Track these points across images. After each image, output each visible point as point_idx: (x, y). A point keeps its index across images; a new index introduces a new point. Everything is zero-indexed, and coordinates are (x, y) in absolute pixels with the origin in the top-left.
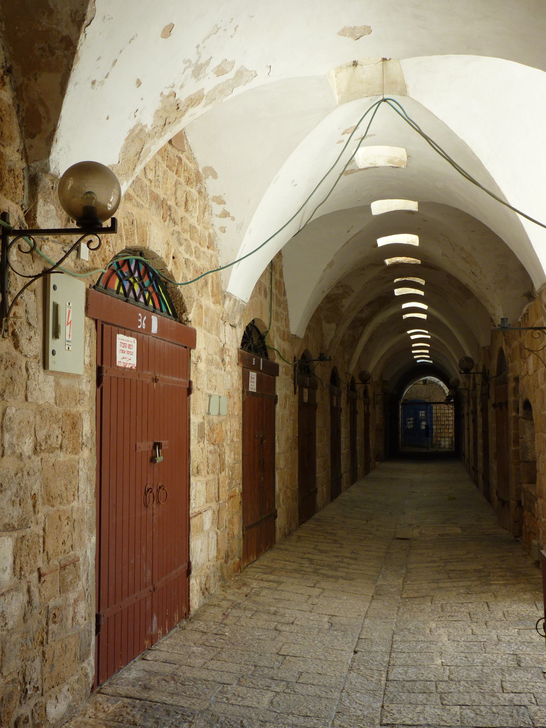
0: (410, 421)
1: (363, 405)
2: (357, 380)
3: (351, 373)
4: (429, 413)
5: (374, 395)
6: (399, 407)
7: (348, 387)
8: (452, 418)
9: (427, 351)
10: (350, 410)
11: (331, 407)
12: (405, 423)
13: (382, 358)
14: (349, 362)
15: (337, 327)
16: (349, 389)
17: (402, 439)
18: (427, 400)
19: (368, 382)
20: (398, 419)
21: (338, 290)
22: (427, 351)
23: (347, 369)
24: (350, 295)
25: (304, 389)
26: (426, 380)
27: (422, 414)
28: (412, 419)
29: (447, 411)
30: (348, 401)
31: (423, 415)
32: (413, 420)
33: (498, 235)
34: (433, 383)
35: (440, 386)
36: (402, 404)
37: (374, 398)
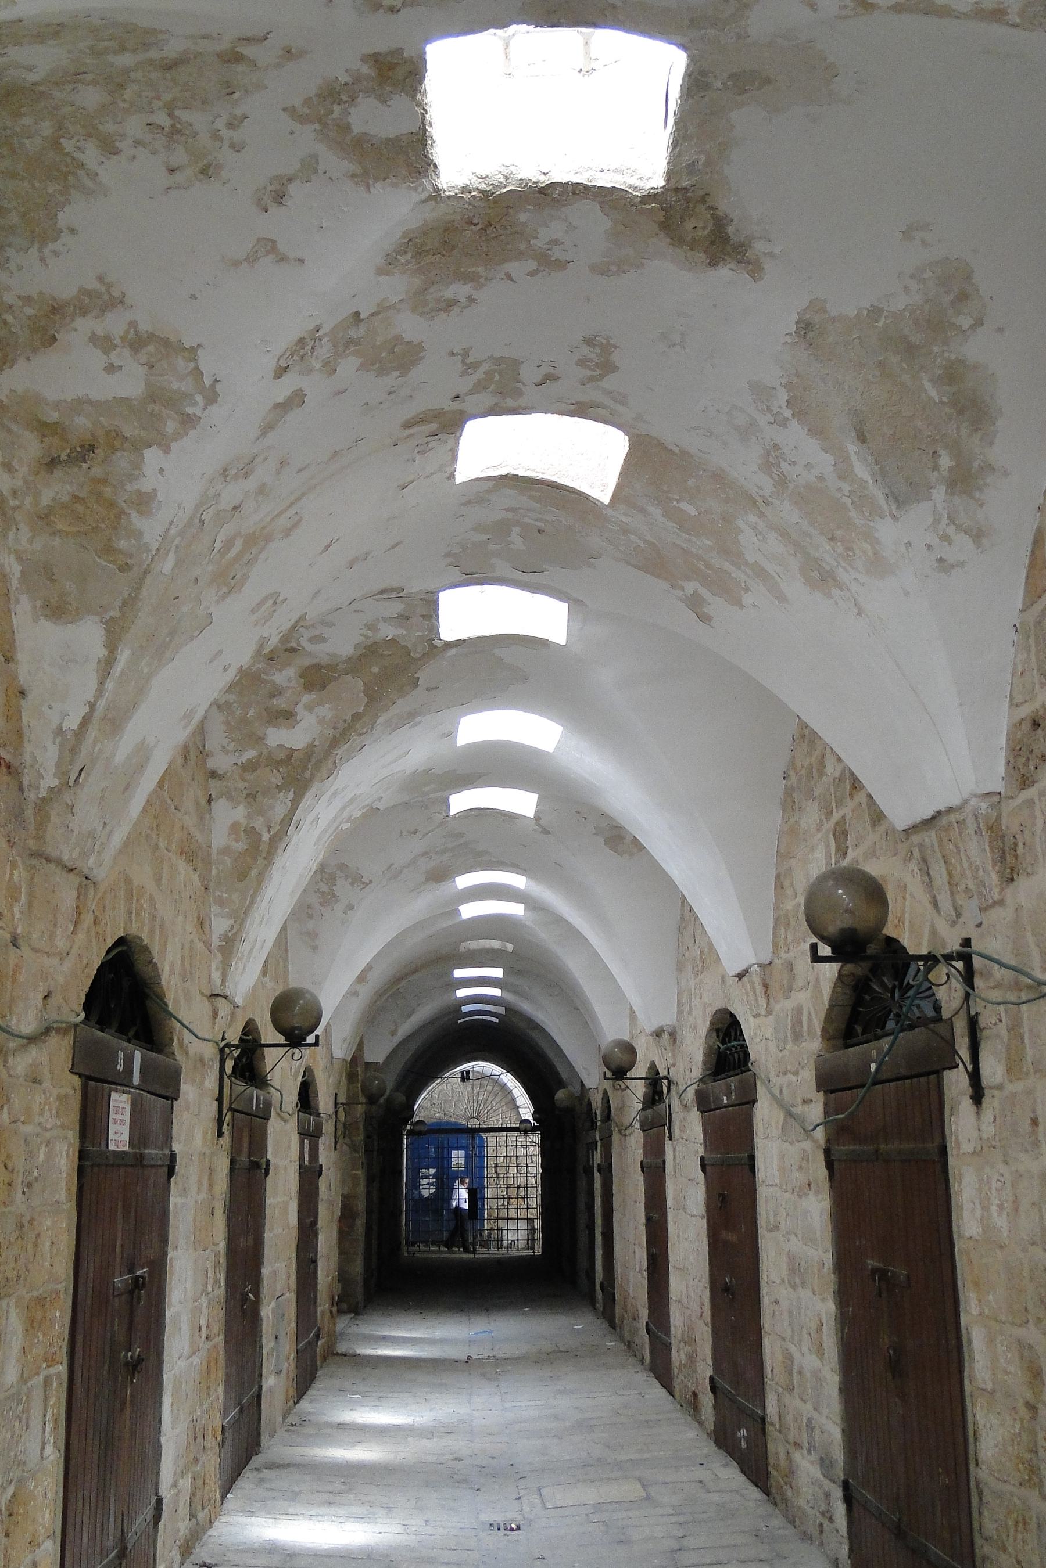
0: (427, 1177)
1: (295, 1138)
2: (269, 1034)
3: (239, 1000)
4: (475, 1158)
5: (336, 1104)
6: (402, 1143)
7: (222, 1062)
8: (536, 1169)
9: (497, 973)
10: (233, 1162)
11: (82, 1155)
12: (415, 1185)
13: (361, 978)
14: (229, 945)
15: (112, 646)
16: (229, 1069)
17: (407, 1224)
18: (473, 1123)
19: (310, 1039)
20: (401, 1172)
21: (111, 369)
22: (497, 973)
23: (216, 976)
24: (189, 421)
25: (114, 1096)
26: (468, 1072)
27: (458, 1158)
28: (433, 1171)
29: (522, 1151)
30: (220, 1122)
31: (462, 1161)
32: (435, 1176)
33: (294, 1255)
34: (483, 1077)
35: (504, 1087)
36: (410, 1133)
37: (336, 1112)
